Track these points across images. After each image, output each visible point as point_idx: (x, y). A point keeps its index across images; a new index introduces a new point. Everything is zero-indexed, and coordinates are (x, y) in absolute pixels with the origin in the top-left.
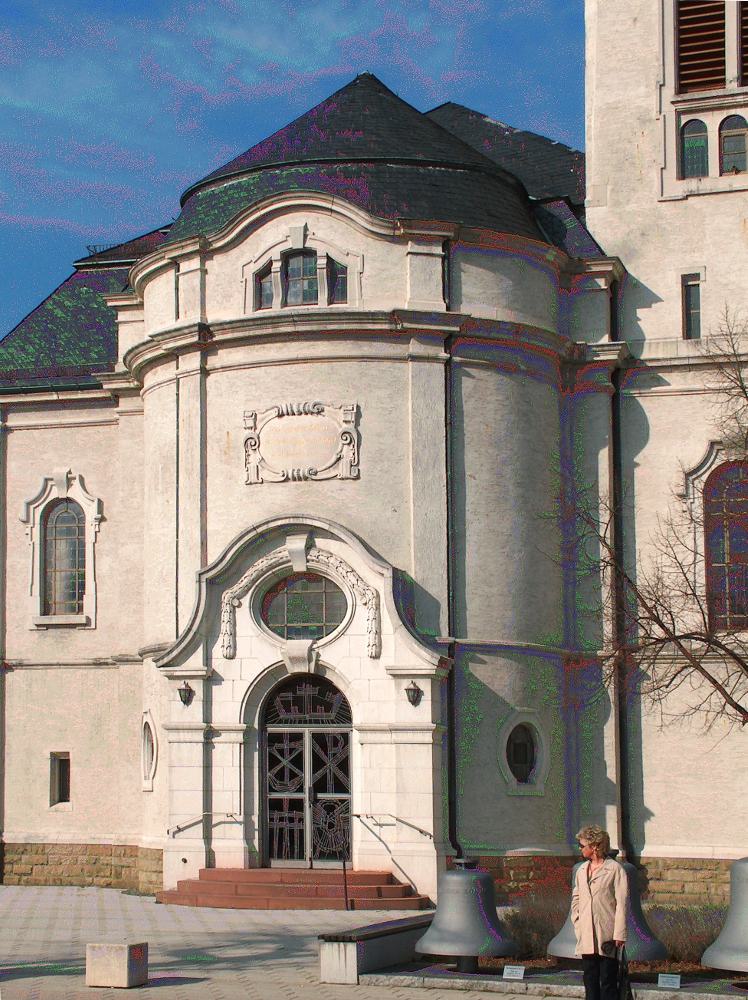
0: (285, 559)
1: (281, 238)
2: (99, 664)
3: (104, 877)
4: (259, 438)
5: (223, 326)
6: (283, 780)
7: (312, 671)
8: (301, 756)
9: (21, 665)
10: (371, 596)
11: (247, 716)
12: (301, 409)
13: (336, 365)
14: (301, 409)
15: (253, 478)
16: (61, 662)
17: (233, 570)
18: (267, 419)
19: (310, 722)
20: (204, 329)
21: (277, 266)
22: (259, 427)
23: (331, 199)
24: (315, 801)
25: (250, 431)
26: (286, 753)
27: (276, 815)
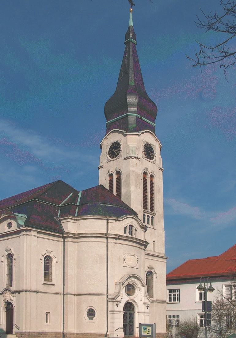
24: (129, 325)
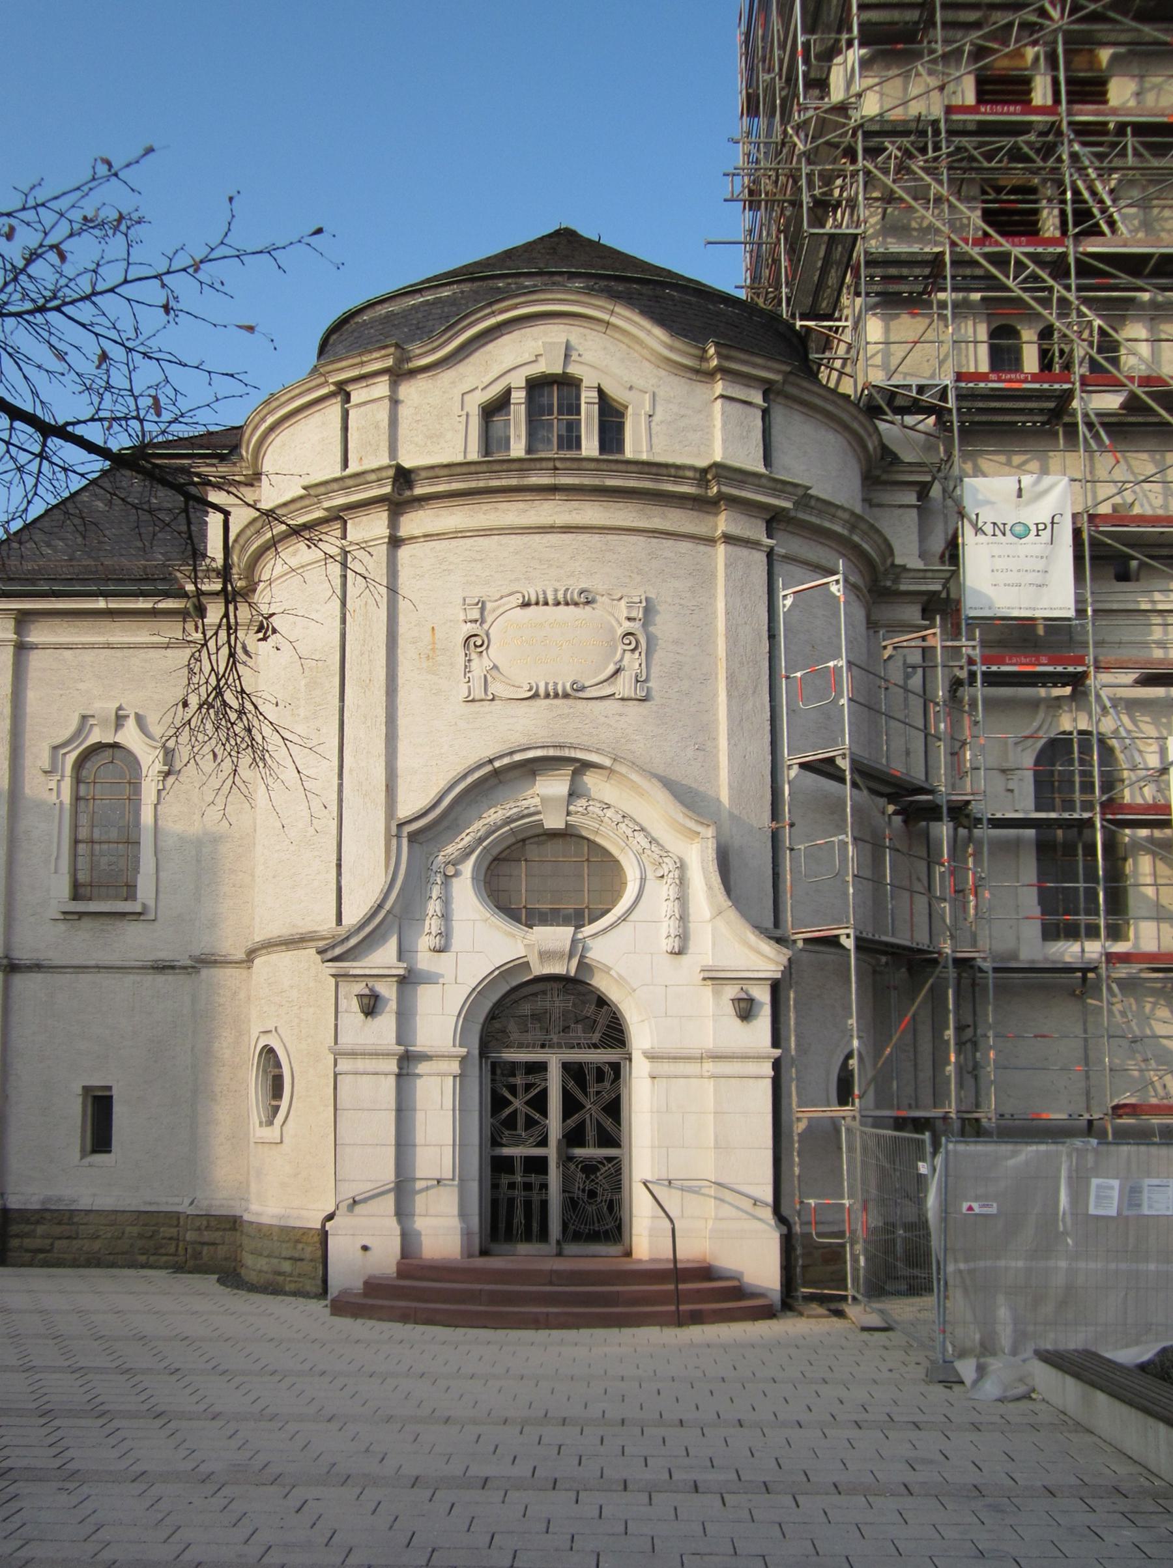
0: (532, 810)
1: (527, 357)
2: (162, 968)
3: (166, 1255)
4: (488, 635)
5: (436, 471)
6: (516, 1129)
7: (572, 973)
8: (544, 1094)
9: (37, 967)
10: (671, 866)
11: (462, 1037)
12: (560, 597)
13: (612, 538)
14: (560, 597)
15: (478, 693)
16: (100, 963)
17: (445, 823)
18: (501, 610)
19: (559, 1046)
20: (403, 477)
21: (518, 396)
22: (489, 619)
23: (611, 307)
24: (566, 1160)
25: (473, 625)
26: (520, 1090)
27: (505, 1180)
